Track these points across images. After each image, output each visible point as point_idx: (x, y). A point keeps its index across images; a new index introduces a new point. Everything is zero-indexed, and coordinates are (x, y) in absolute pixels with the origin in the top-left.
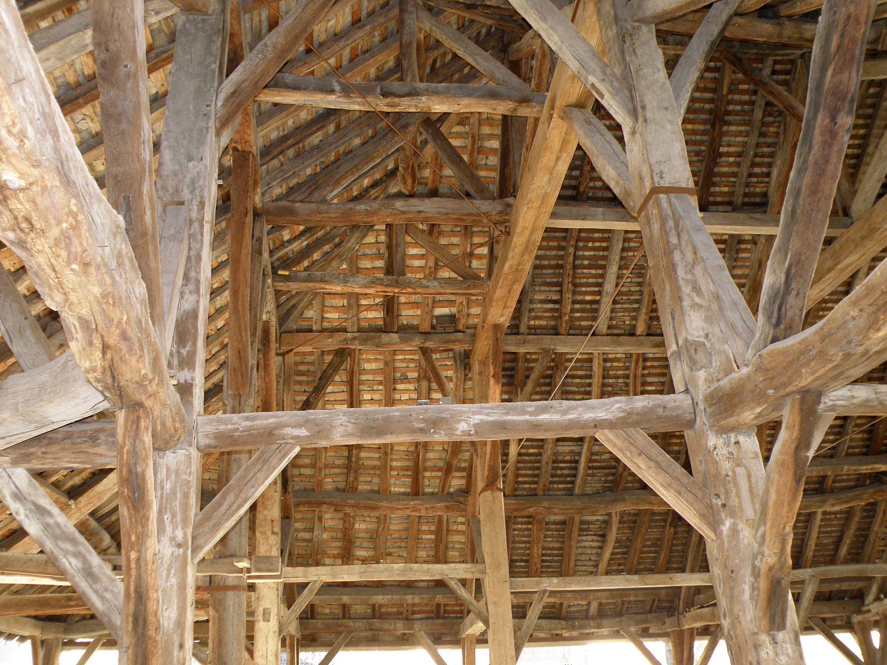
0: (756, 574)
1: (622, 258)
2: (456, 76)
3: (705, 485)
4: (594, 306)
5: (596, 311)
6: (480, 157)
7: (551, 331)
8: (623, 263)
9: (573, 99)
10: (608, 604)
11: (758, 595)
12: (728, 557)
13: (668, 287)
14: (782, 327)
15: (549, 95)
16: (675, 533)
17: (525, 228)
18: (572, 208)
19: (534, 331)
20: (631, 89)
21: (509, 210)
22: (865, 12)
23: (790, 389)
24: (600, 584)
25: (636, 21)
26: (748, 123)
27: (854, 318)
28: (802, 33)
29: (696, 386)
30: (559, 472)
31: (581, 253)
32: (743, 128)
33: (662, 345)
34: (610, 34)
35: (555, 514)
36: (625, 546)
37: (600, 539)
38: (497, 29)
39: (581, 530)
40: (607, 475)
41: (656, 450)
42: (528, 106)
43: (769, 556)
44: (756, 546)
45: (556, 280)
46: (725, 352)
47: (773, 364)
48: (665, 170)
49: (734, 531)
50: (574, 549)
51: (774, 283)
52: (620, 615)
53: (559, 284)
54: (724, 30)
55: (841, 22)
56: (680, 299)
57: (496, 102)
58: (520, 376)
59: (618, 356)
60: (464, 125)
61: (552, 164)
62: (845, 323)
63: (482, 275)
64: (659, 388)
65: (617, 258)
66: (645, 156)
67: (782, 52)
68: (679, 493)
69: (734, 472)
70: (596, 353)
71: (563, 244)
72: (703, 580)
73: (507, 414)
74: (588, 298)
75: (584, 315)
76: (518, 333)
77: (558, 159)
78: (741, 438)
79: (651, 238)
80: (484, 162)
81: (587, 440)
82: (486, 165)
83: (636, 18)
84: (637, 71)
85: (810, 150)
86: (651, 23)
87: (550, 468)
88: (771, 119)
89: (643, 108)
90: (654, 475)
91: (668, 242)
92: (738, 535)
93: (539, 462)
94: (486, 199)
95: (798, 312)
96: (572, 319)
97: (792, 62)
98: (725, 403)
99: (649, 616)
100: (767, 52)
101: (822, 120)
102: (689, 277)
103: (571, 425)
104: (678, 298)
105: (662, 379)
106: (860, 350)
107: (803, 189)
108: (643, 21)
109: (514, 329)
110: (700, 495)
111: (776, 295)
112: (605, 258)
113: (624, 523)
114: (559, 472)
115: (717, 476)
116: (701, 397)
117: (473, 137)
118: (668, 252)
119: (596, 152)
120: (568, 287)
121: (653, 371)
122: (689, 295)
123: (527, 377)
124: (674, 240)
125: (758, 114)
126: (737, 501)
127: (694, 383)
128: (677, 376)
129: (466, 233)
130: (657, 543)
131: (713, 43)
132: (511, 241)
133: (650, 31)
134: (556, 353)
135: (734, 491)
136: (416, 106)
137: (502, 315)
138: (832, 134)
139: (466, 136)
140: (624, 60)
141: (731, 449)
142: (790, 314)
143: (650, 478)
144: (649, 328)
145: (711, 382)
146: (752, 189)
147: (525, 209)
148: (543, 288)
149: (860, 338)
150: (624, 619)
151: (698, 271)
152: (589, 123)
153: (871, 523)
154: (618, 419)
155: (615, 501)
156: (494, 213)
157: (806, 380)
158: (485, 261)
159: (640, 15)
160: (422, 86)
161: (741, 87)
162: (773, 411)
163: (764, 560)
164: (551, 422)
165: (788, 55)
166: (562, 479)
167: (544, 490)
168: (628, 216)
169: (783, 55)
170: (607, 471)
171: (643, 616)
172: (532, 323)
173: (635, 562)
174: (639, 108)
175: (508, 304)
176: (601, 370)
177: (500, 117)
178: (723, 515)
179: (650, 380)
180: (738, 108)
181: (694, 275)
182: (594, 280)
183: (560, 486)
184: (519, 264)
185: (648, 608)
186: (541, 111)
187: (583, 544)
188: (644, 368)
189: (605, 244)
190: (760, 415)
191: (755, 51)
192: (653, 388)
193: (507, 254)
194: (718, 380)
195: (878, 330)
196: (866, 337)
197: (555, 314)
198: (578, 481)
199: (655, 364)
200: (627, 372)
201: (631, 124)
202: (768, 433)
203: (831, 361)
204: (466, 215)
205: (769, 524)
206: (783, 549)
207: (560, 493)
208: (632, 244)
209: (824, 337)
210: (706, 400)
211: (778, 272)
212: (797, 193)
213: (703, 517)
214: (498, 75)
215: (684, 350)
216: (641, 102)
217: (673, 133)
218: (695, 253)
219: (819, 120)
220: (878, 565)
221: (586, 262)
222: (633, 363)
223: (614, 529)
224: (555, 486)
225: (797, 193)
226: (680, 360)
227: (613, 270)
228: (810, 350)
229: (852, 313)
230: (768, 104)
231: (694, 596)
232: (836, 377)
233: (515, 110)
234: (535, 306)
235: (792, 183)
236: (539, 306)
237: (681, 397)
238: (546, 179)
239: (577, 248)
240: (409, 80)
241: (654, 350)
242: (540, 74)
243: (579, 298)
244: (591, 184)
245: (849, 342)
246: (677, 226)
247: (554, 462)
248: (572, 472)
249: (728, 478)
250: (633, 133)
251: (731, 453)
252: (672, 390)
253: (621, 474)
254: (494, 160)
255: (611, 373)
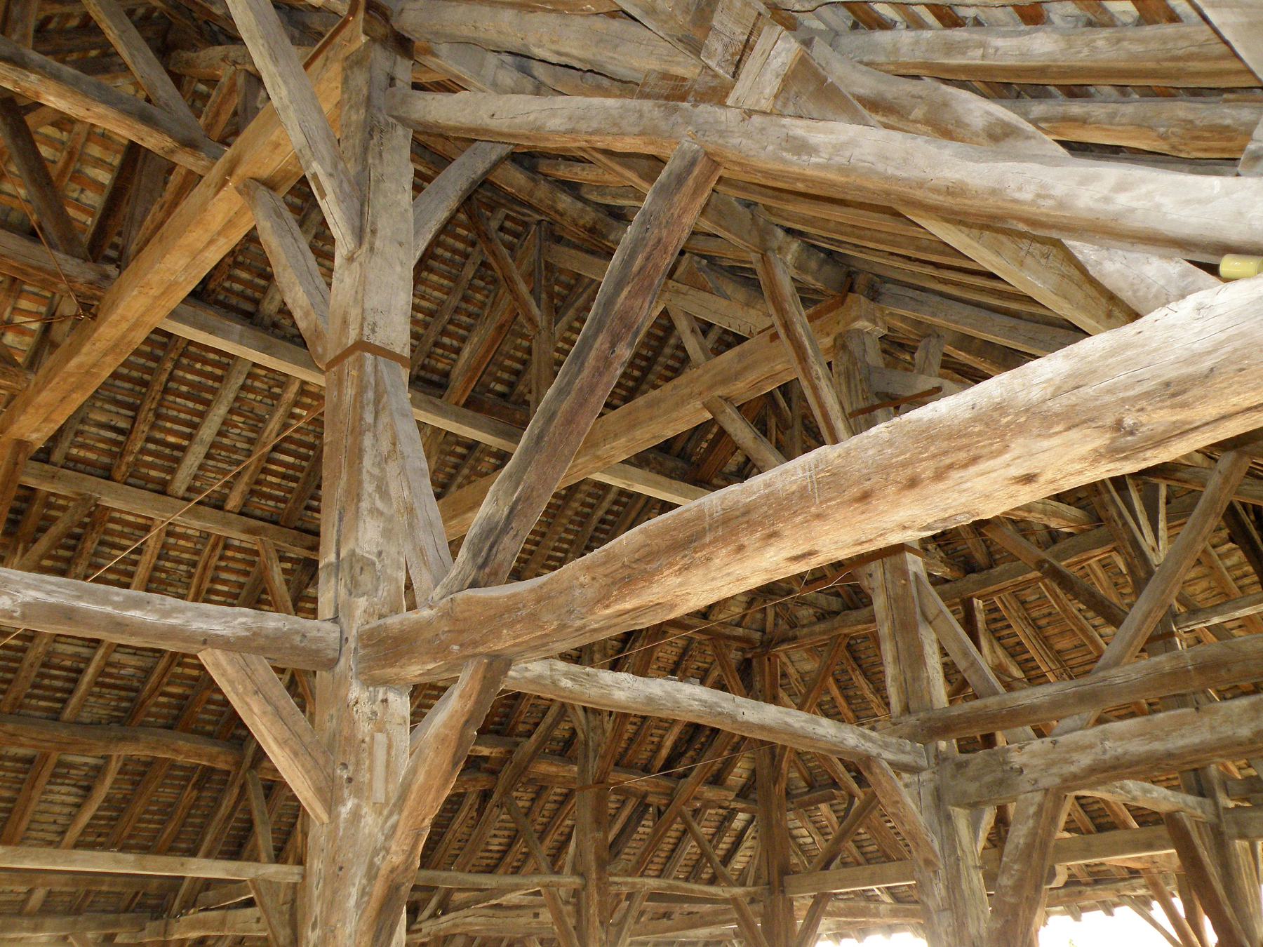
0: (372, 874)
1: (237, 399)
2: (75, 56)
3: (330, 748)
4: (176, 453)
5: (178, 461)
6: (74, 186)
7: (99, 472)
8: (237, 405)
9: (265, 173)
10: (61, 893)
11: (368, 902)
12: (340, 847)
13: (344, 476)
14: (487, 570)
15: (229, 152)
16: (198, 799)
17: (124, 318)
18: (199, 312)
19: (73, 463)
20: (364, 201)
21: (105, 284)
22: (675, 242)
23: (481, 649)
24: (72, 862)
25: (393, 117)
26: (455, 279)
27: (582, 586)
28: (554, 202)
29: (351, 616)
30: (46, 682)
31: (181, 373)
32: (446, 282)
33: (315, 548)
34: (354, 117)
35: (21, 745)
36: (117, 807)
37: (81, 792)
38: (162, 16)
39: (54, 775)
40: (121, 699)
41: (278, 689)
42: (193, 155)
43: (396, 853)
44: (381, 838)
45: (131, 400)
46: (396, 579)
47: (467, 614)
48: (381, 323)
49: (356, 816)
50: (34, 802)
51: (493, 515)
52: (78, 912)
53: (135, 408)
54: (487, 172)
55: (651, 243)
56: (359, 498)
57: (145, 129)
58: (29, 526)
59: (190, 532)
60: (61, 130)
61: (200, 246)
62: (571, 588)
63: (20, 360)
64: (233, 590)
65: (231, 396)
66: (360, 296)
67: (518, 209)
68: (296, 754)
69: (372, 738)
70: (158, 519)
71: (159, 353)
72: (227, 871)
73: (79, 598)
74: (171, 439)
75: (157, 461)
76: (47, 462)
77: (211, 242)
78: (391, 696)
79: (337, 407)
80: (75, 195)
81: (105, 645)
82: (77, 200)
83: (395, 113)
84: (378, 182)
85: (580, 371)
86: (410, 127)
87: (34, 674)
88: (482, 284)
89: (374, 232)
90: (268, 724)
91: (361, 419)
92: (359, 822)
93: (20, 661)
94: (73, 256)
95: (509, 556)
96: (138, 463)
97: (525, 225)
98: (385, 648)
99: (122, 917)
100: (503, 201)
101: (601, 342)
102: (376, 471)
103: (171, 633)
104: (355, 494)
105: (242, 579)
106: (578, 623)
107: (559, 414)
108: (403, 121)
109: (44, 455)
110: (321, 761)
111: (491, 531)
112: (214, 391)
113: (126, 774)
114: (46, 682)
115: (350, 739)
116: (354, 632)
117: (71, 154)
118: (357, 431)
119: (283, 260)
120: (147, 415)
121: (231, 565)
122: (370, 495)
123: (42, 530)
124: (369, 418)
125: (469, 271)
126: (368, 775)
127: (346, 610)
128: (327, 593)
129: (10, 289)
130: (167, 811)
131: (474, 182)
132: (95, 330)
133: (405, 136)
134: (97, 506)
135: (367, 763)
136: (15, 83)
137: (37, 430)
138: (606, 361)
139: (59, 146)
140: (365, 160)
141: (375, 708)
142: (500, 557)
143: (262, 728)
144: (245, 505)
145: (371, 615)
146: (433, 362)
147: (135, 293)
148: (107, 406)
149: (584, 611)
150: (80, 919)
151: (392, 468)
152: (279, 215)
153: (451, 819)
154: (239, 638)
155: (123, 739)
156: (81, 280)
157: (503, 643)
158: (28, 340)
159: (401, 112)
160: (36, 56)
161: (460, 231)
162: (446, 670)
163: (388, 857)
164: (144, 623)
165: (524, 215)
166: (47, 693)
167: (13, 705)
168: (310, 364)
169: (519, 213)
170: (123, 693)
171: (111, 917)
172: (74, 451)
173: (125, 834)
174: (368, 230)
175: (54, 416)
176: (159, 546)
177: (126, 142)
178: (346, 792)
179: (224, 576)
180: (448, 255)
181: (383, 470)
182: (188, 417)
183: (42, 703)
184: (94, 365)
185: (123, 905)
186: (209, 169)
187: (51, 797)
188: (221, 558)
189: (219, 372)
190: (429, 672)
191: (489, 194)
192: (225, 588)
193: (81, 345)
194: (381, 616)
195: (608, 606)
196: (591, 611)
197: (114, 449)
198: (74, 701)
199: (239, 555)
200: (195, 558)
201: (351, 246)
202: (425, 697)
203: (542, 628)
204: (32, 267)
205: (405, 813)
206: (414, 846)
207: (38, 714)
208: (257, 384)
209: (541, 598)
210: (360, 637)
211: (501, 503)
212: (551, 418)
213: (319, 791)
214: (161, 93)
215: (346, 565)
216: (373, 223)
217: (401, 278)
218: (394, 444)
219: (597, 345)
220: (453, 874)
221: (184, 389)
222: (209, 547)
223: (108, 781)
224: (34, 702)
225: (551, 418)
226: (337, 576)
227: (219, 412)
228: (519, 609)
229: (582, 579)
230: (484, 264)
231: (200, 892)
232: (538, 647)
233: (172, 151)
234: (86, 428)
235: (547, 403)
236: (93, 430)
237: (329, 626)
238: (183, 262)
239: (177, 365)
240: (15, 37)
241: (244, 537)
242: (217, 114)
243: (158, 435)
244: (227, 284)
245: (570, 612)
246: (377, 401)
247: (44, 665)
248: (67, 685)
249: (364, 745)
250: (350, 259)
251: (375, 713)
252: (313, 613)
253: (143, 702)
254: (94, 199)
255: (172, 553)
